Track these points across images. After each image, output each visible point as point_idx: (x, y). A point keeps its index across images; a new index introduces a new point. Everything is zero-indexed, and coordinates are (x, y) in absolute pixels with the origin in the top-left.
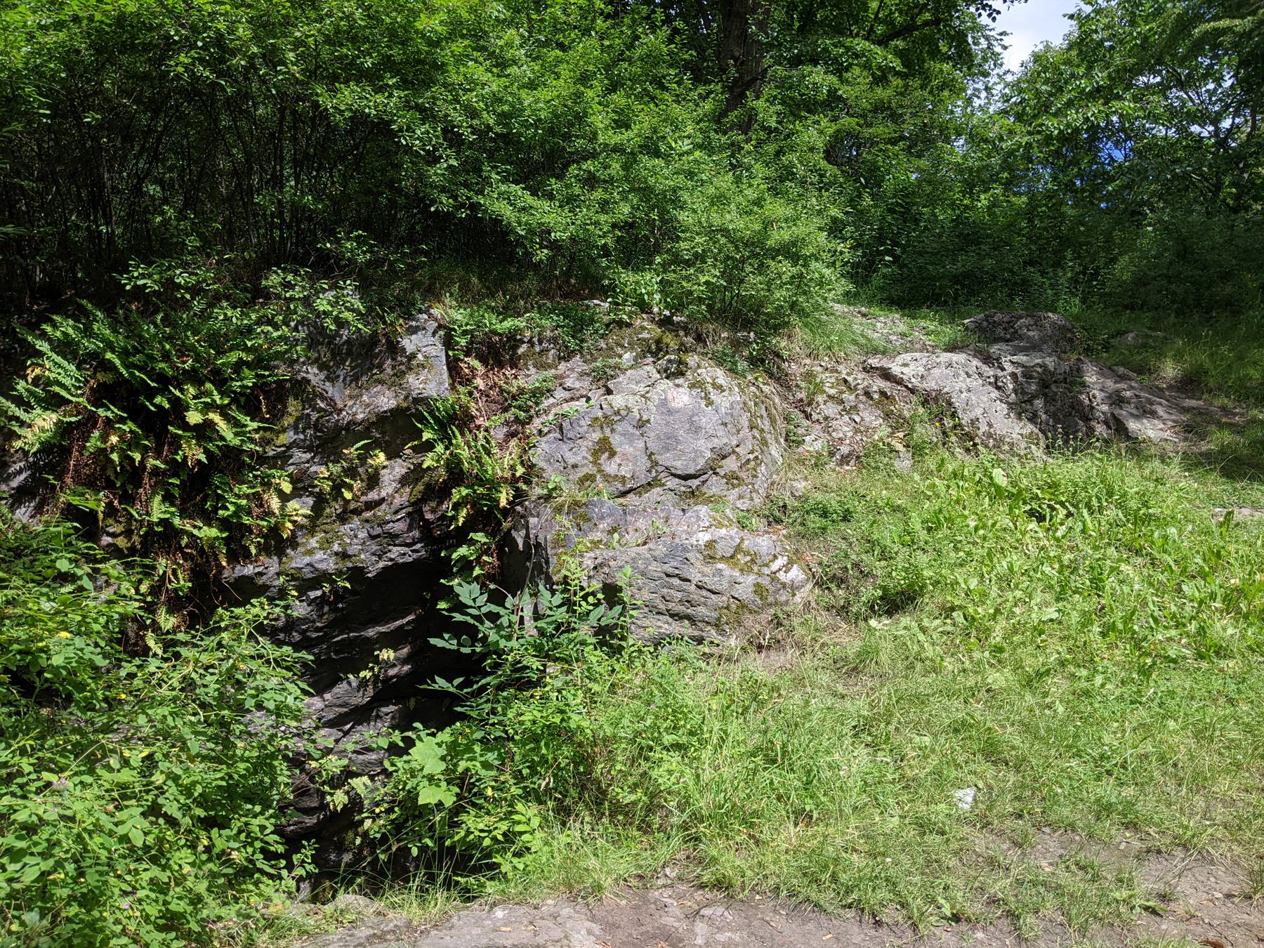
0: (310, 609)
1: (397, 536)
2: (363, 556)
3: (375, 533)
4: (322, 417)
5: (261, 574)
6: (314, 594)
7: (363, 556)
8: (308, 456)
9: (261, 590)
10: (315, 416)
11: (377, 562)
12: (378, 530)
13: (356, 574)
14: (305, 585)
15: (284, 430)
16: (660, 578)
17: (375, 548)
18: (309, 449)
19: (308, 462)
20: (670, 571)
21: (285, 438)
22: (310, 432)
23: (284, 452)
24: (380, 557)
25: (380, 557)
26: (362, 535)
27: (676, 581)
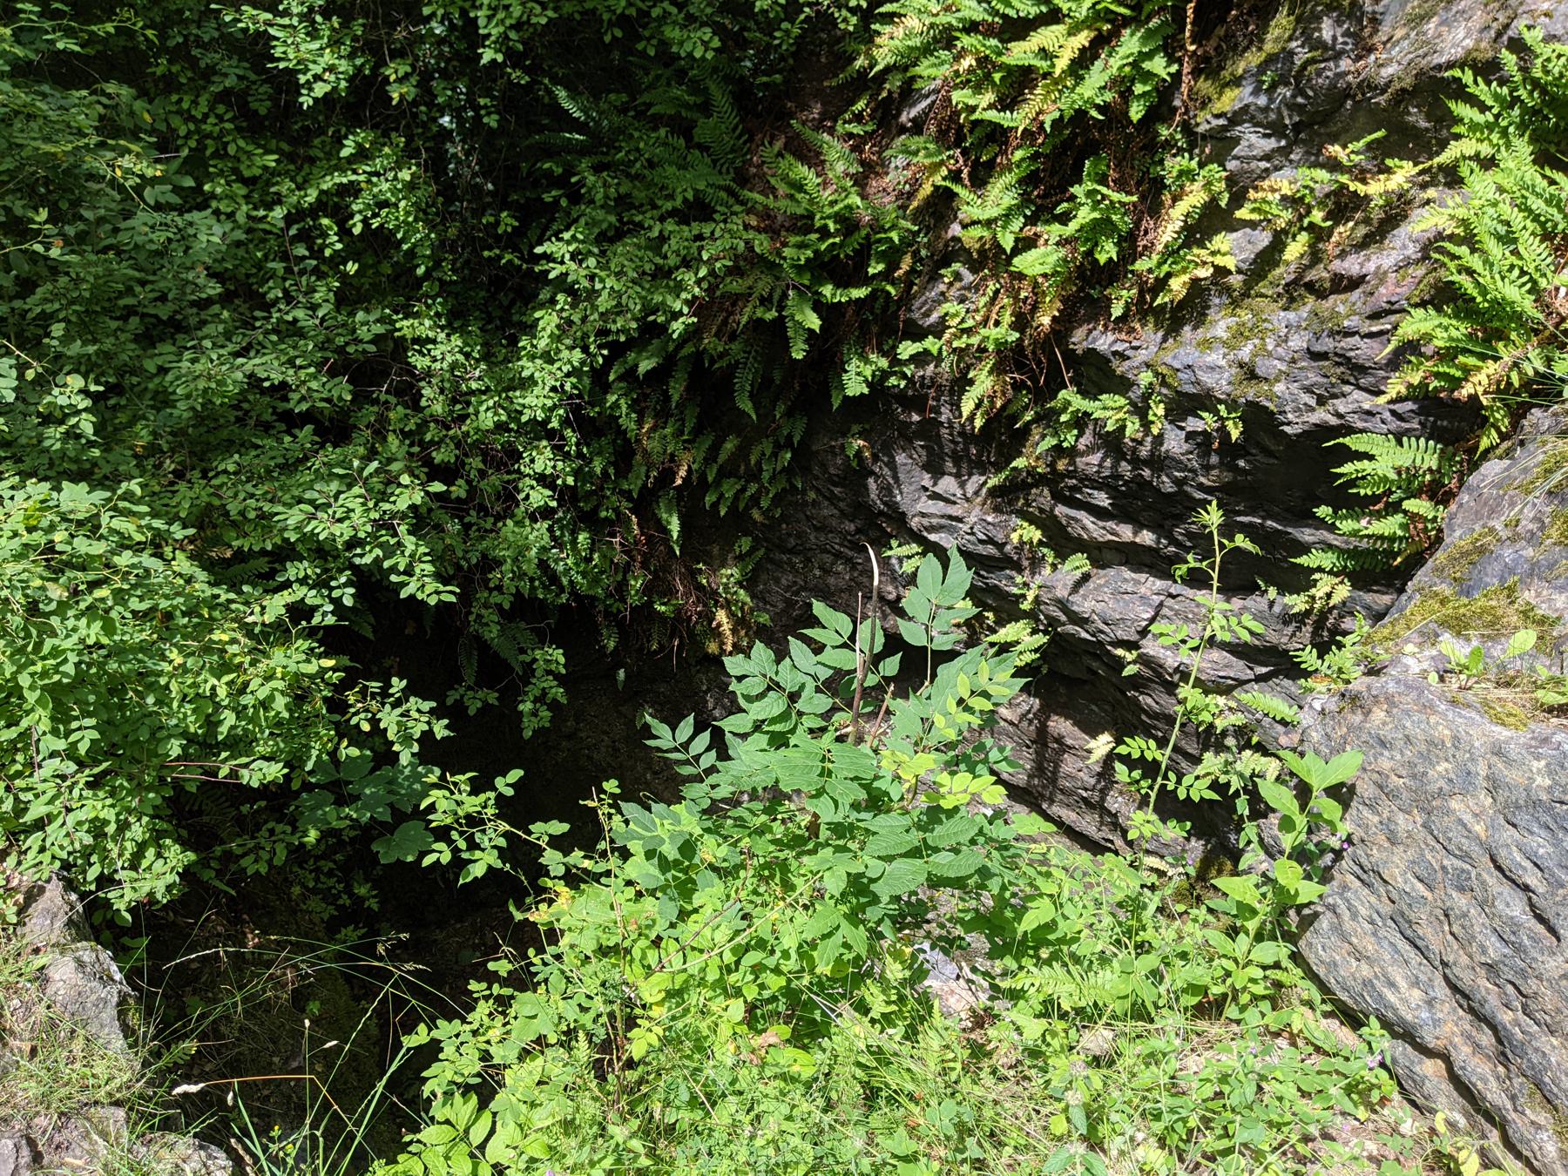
0: (1186, 447)
1: (1362, 370)
2: (1279, 388)
3: (1317, 348)
4: (1313, 61)
5: (1122, 356)
6: (437, 487)
7: (1279, 388)
8: (1272, 144)
9: (1122, 385)
10: (1302, 55)
11: (1311, 409)
12: (1327, 344)
13: (1259, 418)
14: (1185, 404)
15: (1237, 82)
16: (1465, 856)
17: (1313, 378)
18: (1276, 130)
19: (1267, 157)
20: (1513, 858)
21: (1230, 100)
22: (1285, 92)
23: (1224, 128)
24: (1321, 401)
25: (1321, 401)
26: (1298, 342)
27: (1516, 908)
